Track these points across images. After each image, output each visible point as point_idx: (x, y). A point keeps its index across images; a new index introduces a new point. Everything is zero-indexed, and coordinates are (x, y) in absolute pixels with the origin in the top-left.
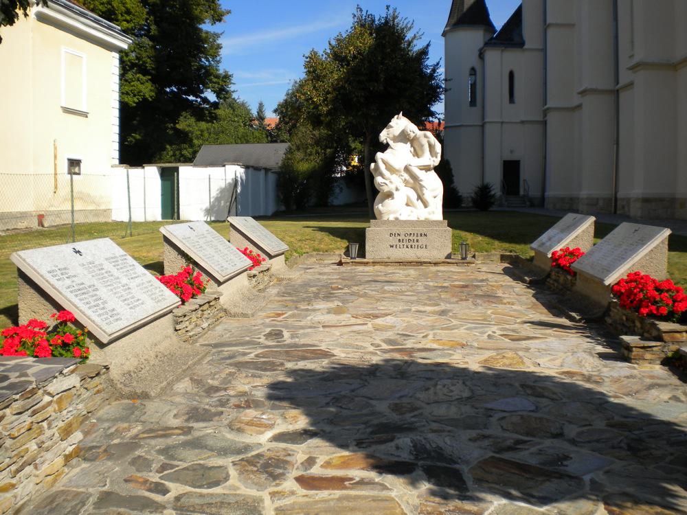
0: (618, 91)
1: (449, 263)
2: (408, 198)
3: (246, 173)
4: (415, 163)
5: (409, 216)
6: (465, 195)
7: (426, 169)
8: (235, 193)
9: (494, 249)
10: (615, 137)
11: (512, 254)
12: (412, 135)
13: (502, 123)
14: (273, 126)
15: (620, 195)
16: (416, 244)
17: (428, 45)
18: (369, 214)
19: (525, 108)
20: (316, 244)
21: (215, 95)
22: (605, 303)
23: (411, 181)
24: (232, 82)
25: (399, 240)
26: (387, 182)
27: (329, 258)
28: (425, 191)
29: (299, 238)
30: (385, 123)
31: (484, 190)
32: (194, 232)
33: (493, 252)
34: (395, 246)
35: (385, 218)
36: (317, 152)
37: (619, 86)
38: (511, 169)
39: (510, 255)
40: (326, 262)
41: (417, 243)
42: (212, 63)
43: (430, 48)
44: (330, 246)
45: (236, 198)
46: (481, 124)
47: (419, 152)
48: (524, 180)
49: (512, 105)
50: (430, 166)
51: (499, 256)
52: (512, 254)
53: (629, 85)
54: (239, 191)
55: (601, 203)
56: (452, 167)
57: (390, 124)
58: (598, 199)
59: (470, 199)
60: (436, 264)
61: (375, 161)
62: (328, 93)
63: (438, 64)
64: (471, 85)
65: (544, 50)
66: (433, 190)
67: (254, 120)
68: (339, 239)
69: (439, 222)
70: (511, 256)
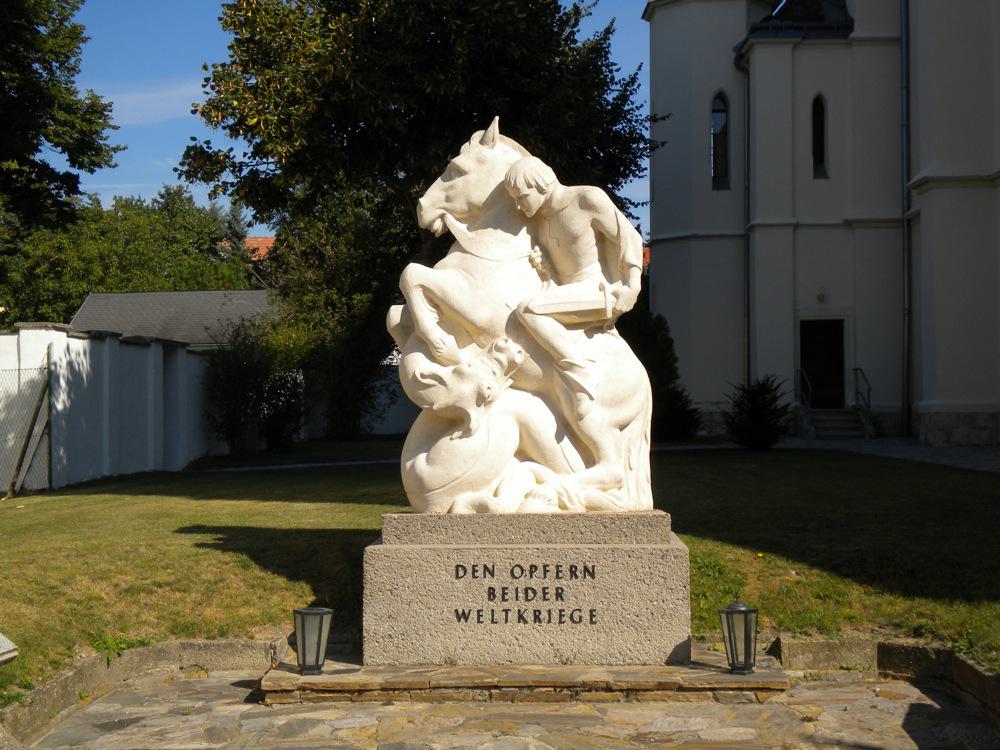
1: (681, 689)
2: (525, 430)
3: (94, 355)
4: (545, 299)
6: (704, 408)
7: (590, 323)
8: (44, 411)
9: (850, 618)
11: (921, 642)
12: (536, 200)
13: (796, 226)
14: (263, 252)
16: (556, 606)
17: (608, 31)
19: (857, 183)
20: (186, 606)
21: (66, 156)
23: (534, 368)
24: (111, 123)
25: (491, 592)
26: (445, 372)
27: (231, 661)
28: (585, 405)
29: (128, 580)
30: (436, 160)
31: (757, 397)
33: (848, 632)
34: (473, 616)
35: (440, 508)
36: (329, 303)
38: (821, 341)
39: (915, 649)
41: (559, 605)
42: (58, 72)
43: (613, 39)
44: (243, 611)
45: (48, 425)
46: (741, 232)
47: (563, 264)
48: (856, 370)
49: (822, 182)
50: (602, 311)
51: (871, 651)
52: (921, 642)
54: (60, 406)
56: (672, 335)
57: (457, 160)
59: (718, 418)
60: (632, 692)
61: (400, 298)
62: (293, 100)
63: (633, 80)
64: (715, 135)
65: (903, 43)
66: (615, 402)
67: (221, 240)
68: (281, 581)
70: (921, 653)
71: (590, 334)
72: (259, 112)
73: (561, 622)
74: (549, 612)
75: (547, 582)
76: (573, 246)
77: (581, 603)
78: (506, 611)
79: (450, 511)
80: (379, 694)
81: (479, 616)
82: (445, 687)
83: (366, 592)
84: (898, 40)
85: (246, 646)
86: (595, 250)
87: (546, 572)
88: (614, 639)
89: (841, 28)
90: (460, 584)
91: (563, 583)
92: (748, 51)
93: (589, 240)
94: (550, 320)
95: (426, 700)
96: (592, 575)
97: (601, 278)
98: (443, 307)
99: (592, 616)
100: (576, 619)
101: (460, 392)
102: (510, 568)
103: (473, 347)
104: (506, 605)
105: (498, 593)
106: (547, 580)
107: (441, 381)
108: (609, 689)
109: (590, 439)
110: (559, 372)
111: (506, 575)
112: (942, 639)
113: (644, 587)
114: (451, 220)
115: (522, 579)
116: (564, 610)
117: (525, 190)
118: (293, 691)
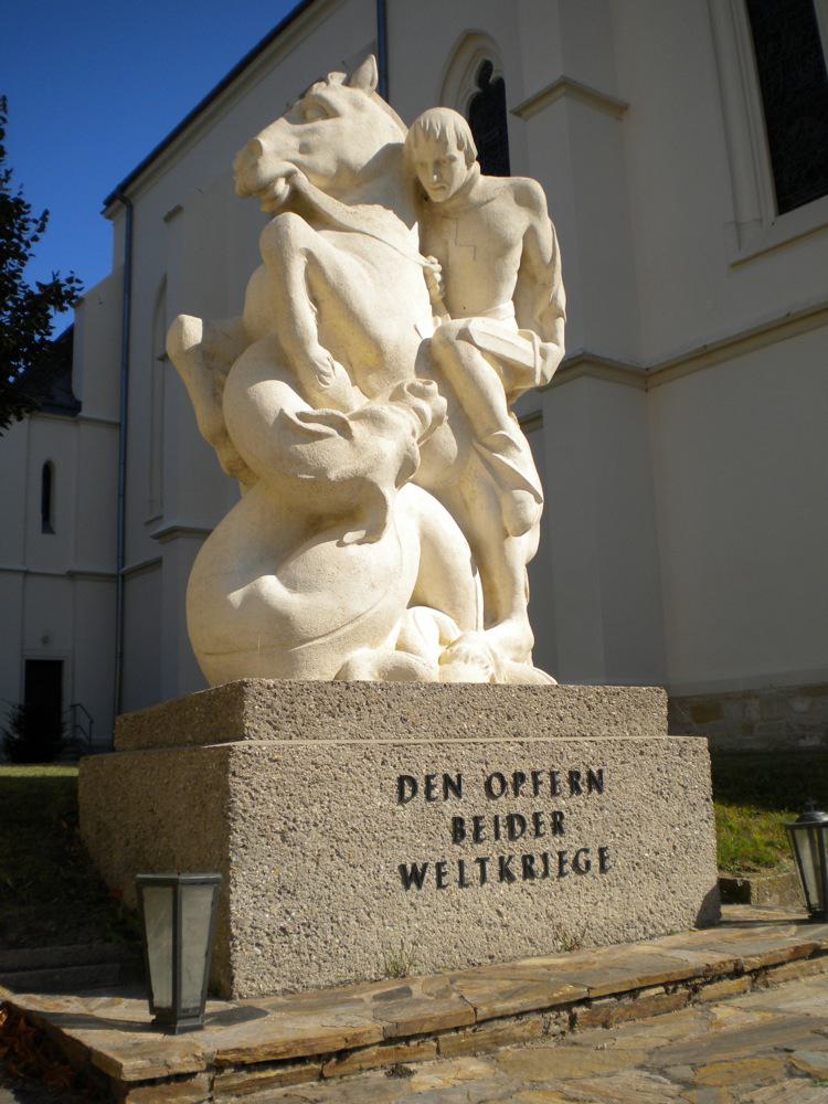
13: (26, 573)
32: (738, 879)
48: (73, 706)
49: (47, 536)
53: (154, 563)
65: (122, 427)
73: (561, 874)
74: (545, 857)
76: (500, 260)
77: (587, 837)
78: (482, 862)
80: (380, 1054)
81: (440, 875)
82: (502, 1017)
83: (237, 838)
87: (536, 783)
88: (632, 895)
90: (405, 813)
91: (561, 803)
98: (328, 306)
99: (602, 859)
100: (583, 866)
102: (483, 779)
105: (469, 827)
106: (538, 799)
108: (737, 973)
110: (480, 455)
111: (479, 791)
115: (502, 799)
116: (565, 852)
118: (193, 1075)
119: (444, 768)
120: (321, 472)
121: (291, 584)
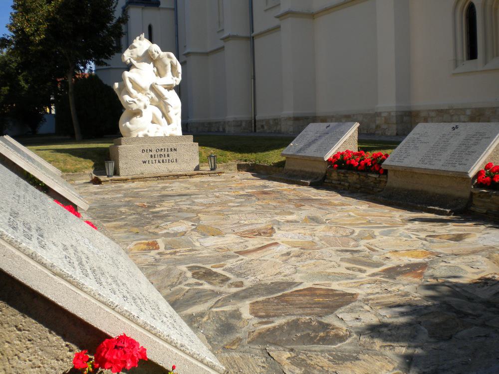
0: (253, 37)
2: (154, 116)
5: (156, 132)
7: (169, 87)
9: (229, 159)
10: (252, 74)
11: (247, 163)
12: (156, 55)
15: (257, 118)
18: (113, 132)
22: (466, 194)
23: (156, 99)
25: (151, 156)
26: (135, 100)
27: (80, 178)
28: (170, 109)
33: (230, 162)
34: (147, 162)
35: (134, 135)
37: (253, 34)
40: (77, 182)
47: (162, 72)
50: (173, 85)
51: (236, 166)
55: (244, 124)
57: (133, 44)
58: (241, 121)
65: (175, 10)
68: (82, 159)
69: (179, 137)
71: (168, 90)
72: (29, 27)
75: (165, 153)
78: (155, 160)
79: (137, 136)
84: (173, 9)
85: (84, 174)
86: (170, 69)
89: (157, 4)
90: (143, 154)
92: (127, 9)
93: (169, 66)
94: (160, 86)
95: (142, 181)
96: (176, 150)
97: (172, 76)
98: (133, 83)
101: (140, 105)
103: (140, 94)
104: (155, 159)
107: (135, 102)
108: (186, 175)
109: (170, 117)
112: (251, 161)
113: (188, 153)
114: (132, 60)
117: (154, 53)
119: (149, 148)
120: (132, 109)
121: (130, 124)
